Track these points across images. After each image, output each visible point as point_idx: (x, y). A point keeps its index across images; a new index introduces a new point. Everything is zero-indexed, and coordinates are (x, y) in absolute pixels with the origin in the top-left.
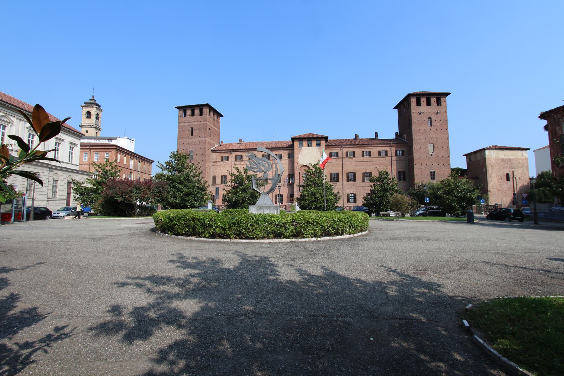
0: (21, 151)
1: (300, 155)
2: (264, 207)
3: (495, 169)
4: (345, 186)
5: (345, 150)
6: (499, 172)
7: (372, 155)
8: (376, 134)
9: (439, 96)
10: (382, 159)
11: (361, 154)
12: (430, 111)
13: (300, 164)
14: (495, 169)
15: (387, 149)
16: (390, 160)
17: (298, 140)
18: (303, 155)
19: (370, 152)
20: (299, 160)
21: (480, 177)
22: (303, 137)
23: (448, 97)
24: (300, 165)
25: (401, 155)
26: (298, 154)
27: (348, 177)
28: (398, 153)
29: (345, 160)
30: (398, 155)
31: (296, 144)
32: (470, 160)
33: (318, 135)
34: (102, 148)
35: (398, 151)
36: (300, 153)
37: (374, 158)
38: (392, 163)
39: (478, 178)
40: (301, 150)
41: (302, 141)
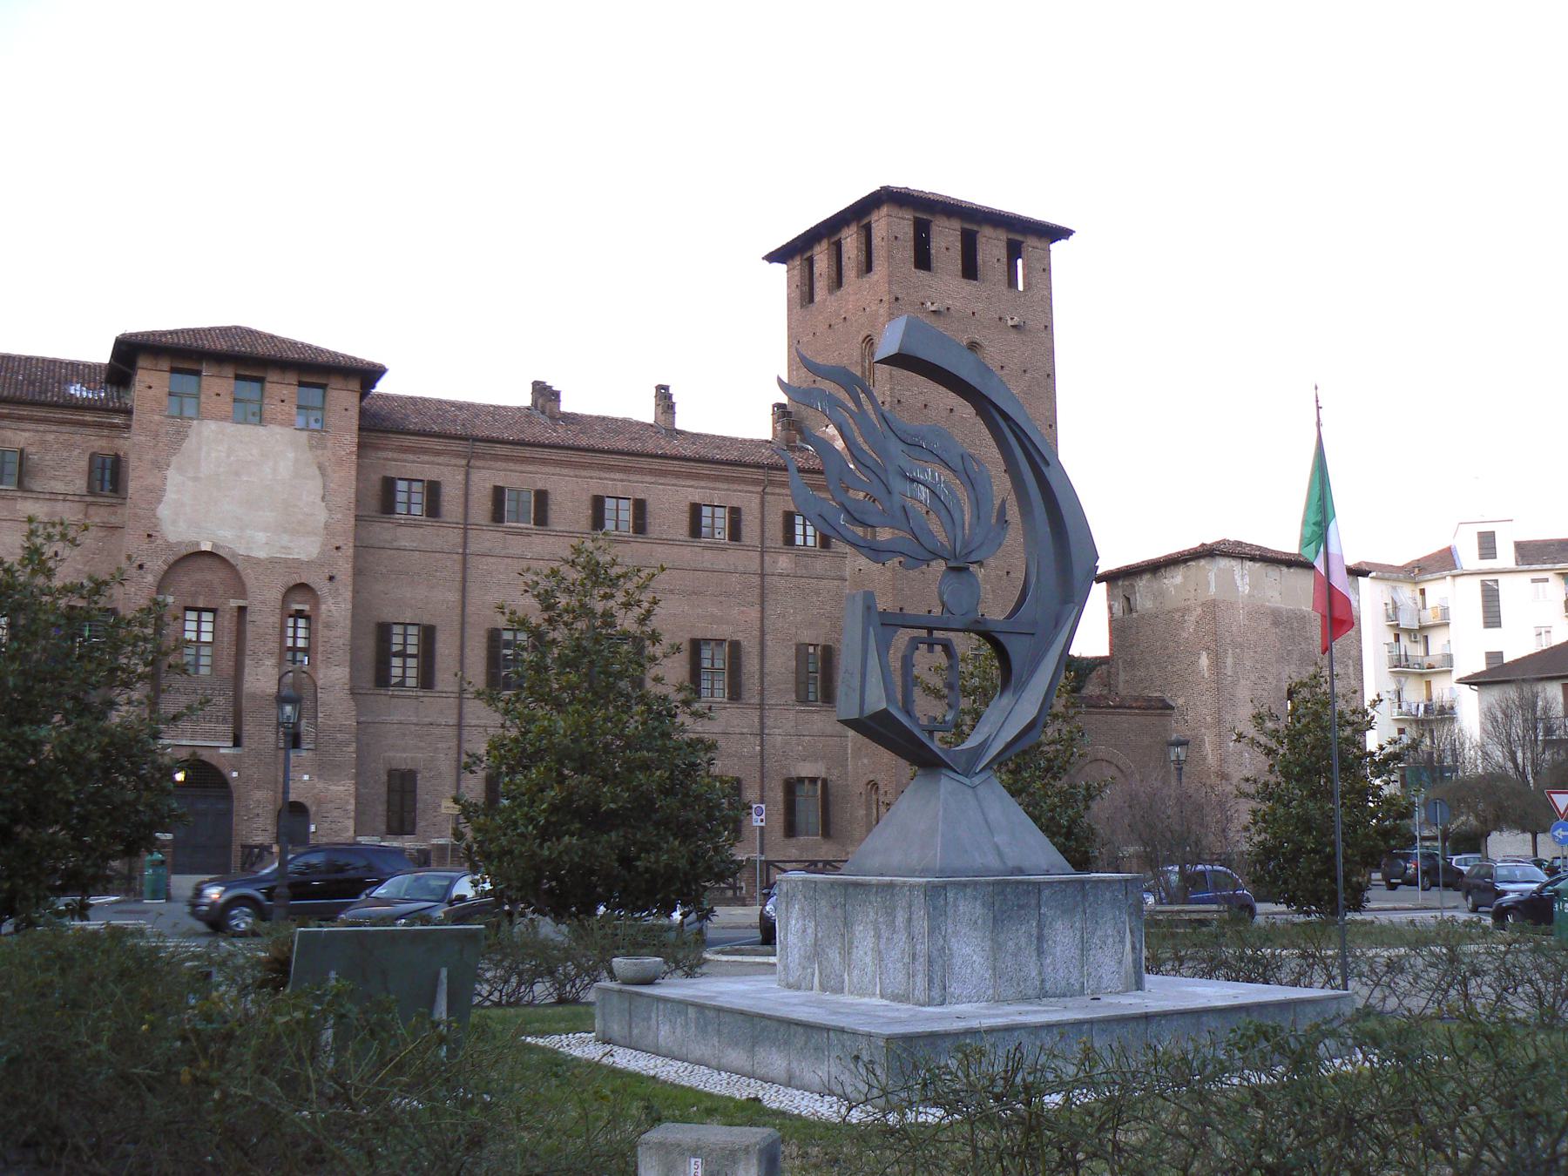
0: (100, 365)
1: (171, 473)
2: (1046, 893)
3: (1248, 664)
4: (474, 722)
5: (486, 479)
6: (1262, 681)
7: (650, 528)
8: (664, 396)
9: (1019, 238)
10: (709, 558)
11: (685, 519)
12: (979, 306)
13: (172, 538)
14: (1248, 664)
15: (748, 500)
16: (755, 566)
17: (165, 364)
18: (196, 479)
19: (542, 497)
20: (164, 511)
21: (1181, 701)
22: (207, 344)
23: (1057, 248)
24: (169, 546)
25: (810, 542)
26: (160, 466)
27: (494, 660)
28: (799, 530)
29: (486, 539)
30: (799, 540)
31: (151, 382)
32: (1130, 608)
33: (302, 344)
34: (186, 366)
35: (799, 520)
36: (174, 460)
37: (660, 548)
38: (762, 587)
39: (1172, 708)
40: (181, 435)
41: (198, 373)
